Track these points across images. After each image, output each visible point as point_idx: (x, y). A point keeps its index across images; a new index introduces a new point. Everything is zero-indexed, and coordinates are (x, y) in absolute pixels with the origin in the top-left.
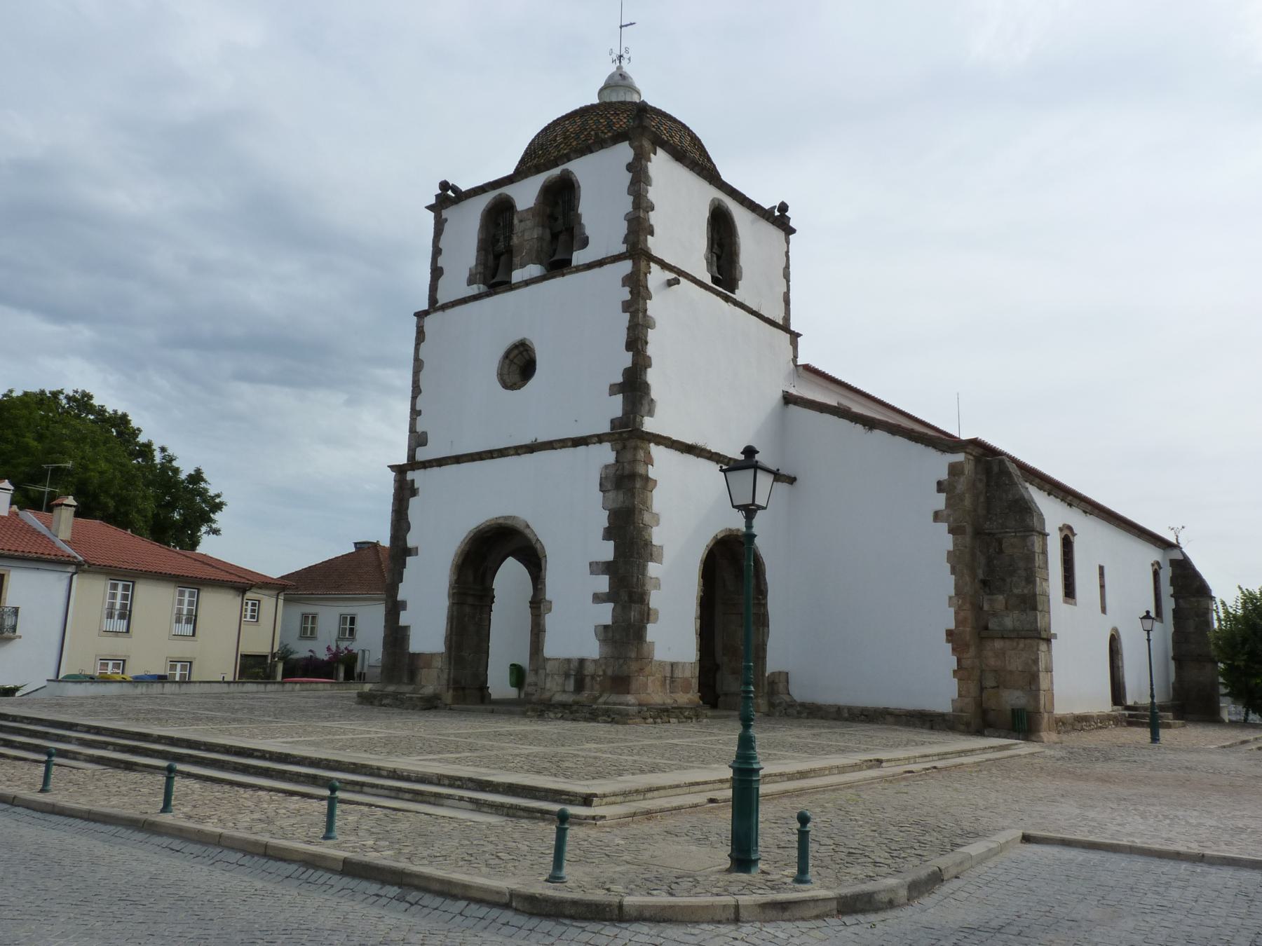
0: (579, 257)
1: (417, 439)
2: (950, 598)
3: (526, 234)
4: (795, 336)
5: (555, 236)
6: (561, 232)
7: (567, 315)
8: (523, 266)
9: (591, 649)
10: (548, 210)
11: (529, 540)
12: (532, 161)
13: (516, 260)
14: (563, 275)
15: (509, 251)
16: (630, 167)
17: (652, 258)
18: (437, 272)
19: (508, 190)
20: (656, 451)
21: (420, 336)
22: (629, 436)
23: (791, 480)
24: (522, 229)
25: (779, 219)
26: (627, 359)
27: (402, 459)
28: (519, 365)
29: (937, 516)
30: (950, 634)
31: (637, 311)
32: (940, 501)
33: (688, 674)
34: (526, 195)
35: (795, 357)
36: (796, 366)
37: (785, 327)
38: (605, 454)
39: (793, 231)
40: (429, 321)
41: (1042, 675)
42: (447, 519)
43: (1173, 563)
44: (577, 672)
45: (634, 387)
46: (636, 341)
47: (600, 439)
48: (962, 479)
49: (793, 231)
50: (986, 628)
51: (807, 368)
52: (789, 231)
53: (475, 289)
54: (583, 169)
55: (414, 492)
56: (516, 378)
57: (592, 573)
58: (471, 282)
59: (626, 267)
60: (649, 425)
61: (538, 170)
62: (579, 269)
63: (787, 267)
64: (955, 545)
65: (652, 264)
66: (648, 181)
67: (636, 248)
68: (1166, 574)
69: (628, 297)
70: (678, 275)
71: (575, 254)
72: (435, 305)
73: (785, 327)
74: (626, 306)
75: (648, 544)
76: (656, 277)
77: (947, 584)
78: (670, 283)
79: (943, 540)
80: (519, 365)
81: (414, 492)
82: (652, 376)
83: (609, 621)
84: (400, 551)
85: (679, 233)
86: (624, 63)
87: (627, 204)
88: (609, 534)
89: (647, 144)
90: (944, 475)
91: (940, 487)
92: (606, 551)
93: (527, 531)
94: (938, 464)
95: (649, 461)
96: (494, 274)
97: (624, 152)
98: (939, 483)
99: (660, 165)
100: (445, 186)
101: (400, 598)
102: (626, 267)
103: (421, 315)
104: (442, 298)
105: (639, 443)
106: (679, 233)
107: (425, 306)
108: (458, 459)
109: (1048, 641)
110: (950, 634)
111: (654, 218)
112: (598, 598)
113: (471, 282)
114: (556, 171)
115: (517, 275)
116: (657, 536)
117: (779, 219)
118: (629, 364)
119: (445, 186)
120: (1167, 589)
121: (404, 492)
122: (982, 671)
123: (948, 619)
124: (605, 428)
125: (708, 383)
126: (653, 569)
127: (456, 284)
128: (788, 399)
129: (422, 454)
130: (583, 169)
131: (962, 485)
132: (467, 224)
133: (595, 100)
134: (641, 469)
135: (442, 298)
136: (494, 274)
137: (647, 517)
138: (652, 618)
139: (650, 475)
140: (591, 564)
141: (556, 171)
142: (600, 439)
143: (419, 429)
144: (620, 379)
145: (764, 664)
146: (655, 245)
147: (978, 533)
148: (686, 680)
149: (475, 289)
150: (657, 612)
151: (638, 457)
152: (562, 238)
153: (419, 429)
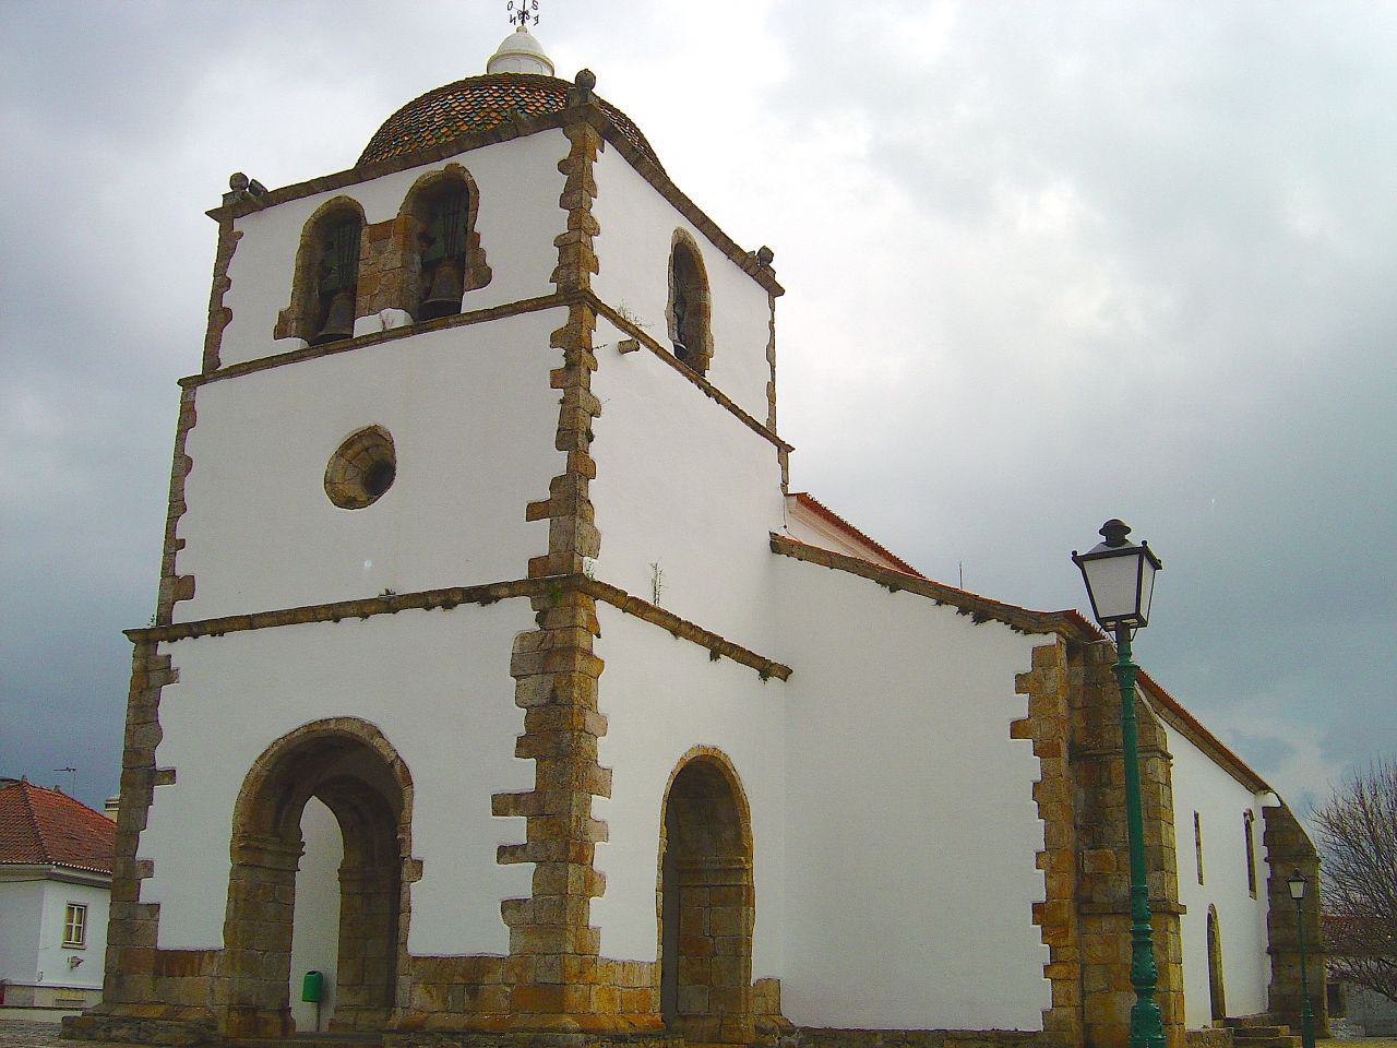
0: (472, 301)
1: (178, 587)
2: (420, 874)
3: (384, 263)
4: (784, 449)
5: (429, 268)
6: (439, 261)
7: (455, 392)
8: (371, 311)
9: (496, 940)
10: (419, 227)
11: (381, 758)
12: (395, 144)
13: (362, 301)
14: (449, 326)
15: (352, 292)
16: (563, 166)
17: (598, 307)
18: (220, 316)
19: (353, 192)
20: (604, 611)
21: (188, 417)
22: (561, 587)
23: (785, 673)
24: (388, 244)
25: (759, 266)
26: (559, 463)
27: (146, 620)
28: (366, 468)
29: (1017, 729)
30: (1037, 908)
31: (576, 385)
32: (1020, 706)
33: (646, 981)
34: (383, 201)
35: (785, 484)
36: (786, 495)
37: (767, 432)
38: (519, 615)
39: (781, 292)
40: (203, 394)
41: (1172, 967)
42: (225, 722)
43: (1267, 811)
44: (468, 974)
45: (566, 503)
46: (573, 434)
47: (513, 589)
48: (1055, 671)
49: (781, 292)
50: (1089, 901)
51: (805, 500)
52: (775, 291)
53: (294, 344)
54: (484, 166)
55: (170, 675)
56: (354, 489)
57: (496, 813)
58: (280, 333)
59: (560, 316)
60: (598, 568)
61: (407, 163)
62: (368, 340)
63: (771, 346)
64: (1044, 773)
65: (600, 317)
66: (592, 189)
67: (573, 290)
68: (1259, 826)
69: (561, 363)
70: (636, 339)
71: (467, 295)
72: (213, 368)
73: (767, 432)
74: (557, 379)
75: (591, 761)
76: (605, 334)
77: (1034, 832)
78: (624, 349)
79: (1025, 763)
80: (366, 468)
81: (170, 675)
82: (596, 490)
83: (526, 891)
84: (142, 775)
85: (633, 277)
86: (529, 23)
87: (560, 221)
88: (524, 747)
89: (592, 135)
90: (1026, 666)
91: (1022, 683)
92: (523, 775)
93: (377, 742)
94: (1015, 651)
95: (594, 629)
96: (323, 317)
97: (556, 144)
98: (1020, 678)
99: (608, 166)
100: (238, 180)
101: (141, 855)
102: (560, 316)
103: (189, 384)
104: (228, 358)
105: (581, 598)
106: (633, 277)
107: (197, 370)
108: (251, 622)
109: (1176, 915)
110: (1037, 908)
111: (599, 245)
112: (506, 853)
113: (280, 333)
114: (439, 166)
115: (364, 325)
116: (607, 751)
117: (759, 266)
118: (561, 470)
119: (238, 180)
120: (1261, 852)
121: (151, 676)
122: (1083, 966)
123: (1036, 887)
124: (522, 573)
125: (670, 508)
126: (599, 806)
127: (251, 336)
128: (778, 545)
129: (183, 613)
130: (484, 166)
131: (1055, 680)
132: (277, 247)
133: (481, 72)
134: (582, 639)
135: (228, 358)
136: (323, 317)
137: (589, 717)
138: (597, 887)
139: (595, 652)
140: (494, 797)
141: (439, 166)
142: (513, 589)
143: (181, 570)
144: (544, 494)
145: (748, 967)
146: (600, 286)
147: (1077, 754)
148: (644, 990)
149: (294, 344)
150: (602, 877)
151: (579, 621)
152: (446, 270)
153: (180, 571)
